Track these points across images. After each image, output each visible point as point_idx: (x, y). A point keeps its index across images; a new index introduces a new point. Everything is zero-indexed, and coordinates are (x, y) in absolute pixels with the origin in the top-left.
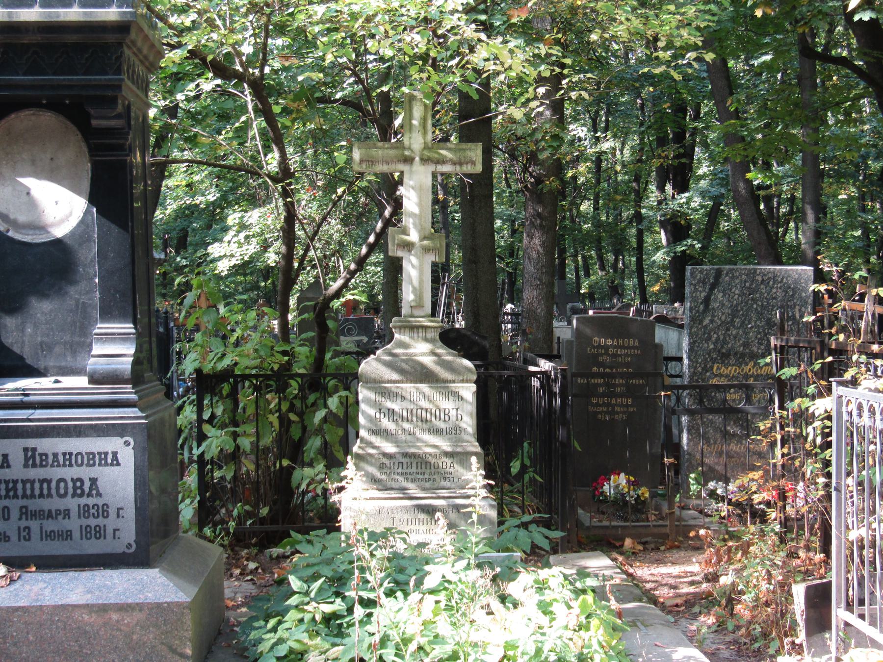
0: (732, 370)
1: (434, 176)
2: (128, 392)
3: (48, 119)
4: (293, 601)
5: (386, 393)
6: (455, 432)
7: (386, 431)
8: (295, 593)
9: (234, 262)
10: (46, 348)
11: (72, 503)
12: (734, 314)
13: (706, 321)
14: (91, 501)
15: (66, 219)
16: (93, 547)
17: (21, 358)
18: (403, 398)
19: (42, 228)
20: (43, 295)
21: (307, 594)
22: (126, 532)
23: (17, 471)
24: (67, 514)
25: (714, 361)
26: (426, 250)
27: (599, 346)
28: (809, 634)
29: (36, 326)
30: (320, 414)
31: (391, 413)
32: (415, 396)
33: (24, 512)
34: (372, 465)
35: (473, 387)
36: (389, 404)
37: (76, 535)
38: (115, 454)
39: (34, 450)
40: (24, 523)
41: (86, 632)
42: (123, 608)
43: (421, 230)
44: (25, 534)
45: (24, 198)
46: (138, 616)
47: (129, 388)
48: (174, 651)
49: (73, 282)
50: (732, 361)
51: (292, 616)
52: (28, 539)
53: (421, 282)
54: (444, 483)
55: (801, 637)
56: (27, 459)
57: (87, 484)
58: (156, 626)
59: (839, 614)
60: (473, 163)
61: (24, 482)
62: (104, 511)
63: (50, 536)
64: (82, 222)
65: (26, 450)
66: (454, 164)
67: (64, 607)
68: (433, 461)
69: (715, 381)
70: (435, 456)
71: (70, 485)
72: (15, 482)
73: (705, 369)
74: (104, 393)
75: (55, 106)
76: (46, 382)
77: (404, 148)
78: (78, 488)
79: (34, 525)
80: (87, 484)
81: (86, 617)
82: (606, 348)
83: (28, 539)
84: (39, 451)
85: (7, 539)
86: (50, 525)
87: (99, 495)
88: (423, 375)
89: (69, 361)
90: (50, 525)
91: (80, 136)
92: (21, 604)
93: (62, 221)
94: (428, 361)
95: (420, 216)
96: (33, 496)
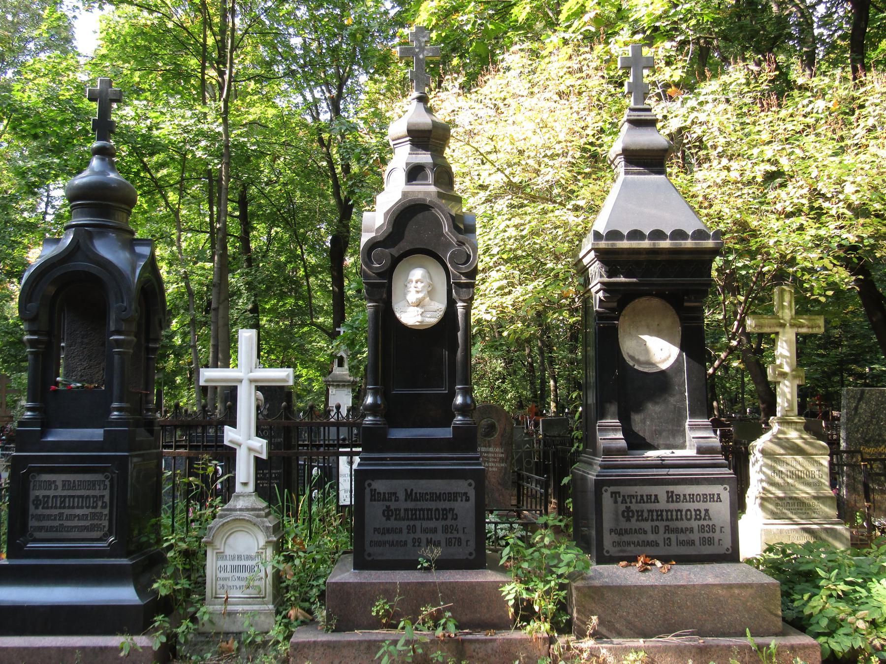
0: (871, 450)
1: (797, 334)
2: (720, 459)
3: (656, 302)
5: (777, 461)
6: (817, 485)
7: (778, 484)
8: (823, 578)
10: (658, 433)
11: (695, 524)
13: (856, 421)
14: (705, 523)
16: (707, 550)
17: (644, 439)
19: (653, 365)
20: (656, 403)
21: (829, 579)
23: (663, 505)
24: (691, 530)
25: (861, 444)
26: (795, 377)
29: (652, 420)
32: (794, 464)
33: (667, 529)
34: (771, 504)
35: (828, 458)
36: (779, 468)
37: (697, 543)
38: (718, 495)
39: (672, 492)
40: (667, 536)
41: (720, 601)
42: (741, 586)
47: (720, 456)
50: (872, 444)
53: (792, 396)
56: (668, 498)
57: (703, 513)
58: (761, 597)
60: (819, 327)
62: (713, 529)
63: (682, 543)
64: (677, 360)
65: (667, 492)
67: (707, 585)
70: (808, 499)
71: (693, 513)
72: (662, 511)
74: (706, 459)
75: (660, 295)
79: (673, 537)
80: (703, 513)
84: (676, 493)
85: (657, 545)
86: (682, 537)
89: (671, 441)
90: (682, 537)
91: (674, 312)
94: (799, 442)
95: (790, 358)
96: (672, 519)
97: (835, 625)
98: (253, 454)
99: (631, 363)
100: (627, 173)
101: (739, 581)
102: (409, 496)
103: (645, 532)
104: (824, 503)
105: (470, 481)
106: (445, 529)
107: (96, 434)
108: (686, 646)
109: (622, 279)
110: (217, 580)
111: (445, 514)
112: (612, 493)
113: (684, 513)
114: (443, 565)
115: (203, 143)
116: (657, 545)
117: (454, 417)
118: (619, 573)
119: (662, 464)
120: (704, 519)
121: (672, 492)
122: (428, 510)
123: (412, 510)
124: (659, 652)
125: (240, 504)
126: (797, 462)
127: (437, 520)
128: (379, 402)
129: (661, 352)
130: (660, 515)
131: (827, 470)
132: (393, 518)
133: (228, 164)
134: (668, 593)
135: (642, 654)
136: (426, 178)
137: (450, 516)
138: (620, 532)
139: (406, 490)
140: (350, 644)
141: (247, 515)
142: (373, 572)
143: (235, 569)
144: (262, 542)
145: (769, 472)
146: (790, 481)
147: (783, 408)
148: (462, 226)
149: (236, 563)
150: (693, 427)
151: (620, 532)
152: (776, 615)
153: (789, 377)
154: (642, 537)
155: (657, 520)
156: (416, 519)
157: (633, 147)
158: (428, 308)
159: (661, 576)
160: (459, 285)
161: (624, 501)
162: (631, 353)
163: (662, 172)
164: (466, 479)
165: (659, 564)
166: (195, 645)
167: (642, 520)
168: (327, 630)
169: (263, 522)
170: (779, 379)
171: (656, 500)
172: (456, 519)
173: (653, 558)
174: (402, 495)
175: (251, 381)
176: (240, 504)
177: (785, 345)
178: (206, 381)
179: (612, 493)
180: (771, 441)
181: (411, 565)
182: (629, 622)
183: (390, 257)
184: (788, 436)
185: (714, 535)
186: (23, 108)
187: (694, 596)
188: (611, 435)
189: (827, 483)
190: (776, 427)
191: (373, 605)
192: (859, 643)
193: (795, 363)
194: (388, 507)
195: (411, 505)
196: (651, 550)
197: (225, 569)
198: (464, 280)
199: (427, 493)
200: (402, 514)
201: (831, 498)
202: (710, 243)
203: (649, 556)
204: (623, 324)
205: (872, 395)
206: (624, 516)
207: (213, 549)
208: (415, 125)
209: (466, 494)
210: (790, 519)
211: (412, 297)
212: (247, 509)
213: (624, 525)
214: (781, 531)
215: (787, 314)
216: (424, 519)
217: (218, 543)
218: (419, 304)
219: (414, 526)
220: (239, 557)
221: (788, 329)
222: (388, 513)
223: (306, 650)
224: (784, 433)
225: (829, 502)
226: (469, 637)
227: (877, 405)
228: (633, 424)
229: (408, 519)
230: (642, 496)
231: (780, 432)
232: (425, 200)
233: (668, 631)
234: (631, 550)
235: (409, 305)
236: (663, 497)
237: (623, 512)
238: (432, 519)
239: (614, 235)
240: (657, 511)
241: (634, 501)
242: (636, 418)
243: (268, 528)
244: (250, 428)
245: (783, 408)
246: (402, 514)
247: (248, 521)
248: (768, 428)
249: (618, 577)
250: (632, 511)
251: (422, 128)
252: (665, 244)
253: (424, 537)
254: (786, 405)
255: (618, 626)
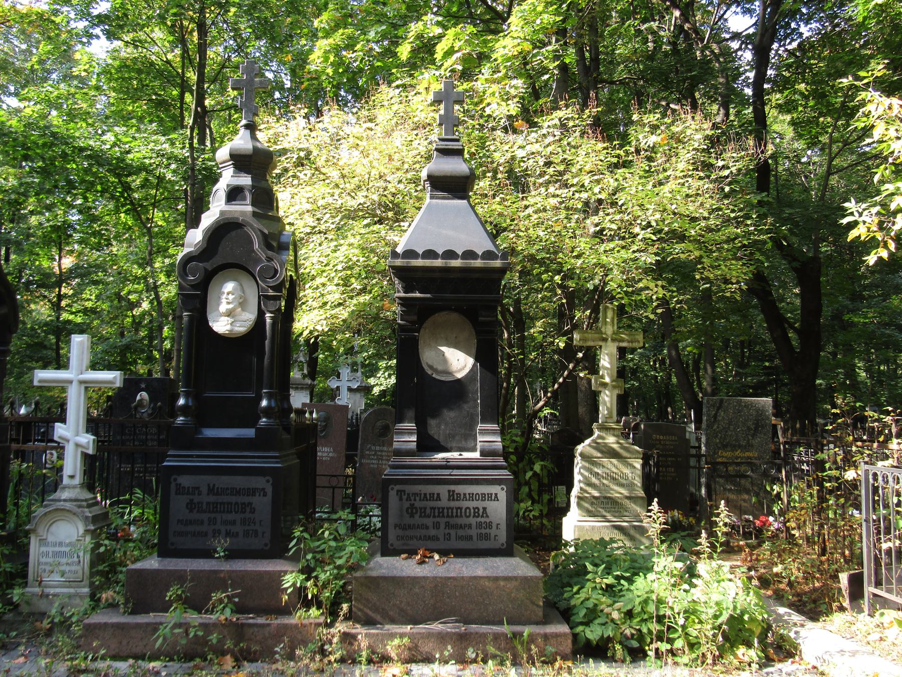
0: (729, 454)
2: (501, 461)
3: (454, 316)
4: (589, 576)
6: (630, 486)
8: (590, 572)
9: (382, 388)
10: (452, 436)
11: (473, 521)
12: (730, 423)
13: (715, 427)
14: (483, 520)
15: (463, 368)
17: (439, 442)
18: (603, 467)
19: (450, 373)
20: (451, 409)
21: (596, 573)
22: (501, 536)
23: (444, 502)
24: (470, 526)
25: (719, 448)
26: (614, 387)
27: (656, 440)
28: (851, 601)
30: (529, 474)
31: (597, 475)
32: (610, 466)
35: (641, 461)
36: (596, 470)
37: (475, 538)
38: (496, 494)
39: (454, 491)
40: (447, 531)
42: (507, 579)
43: (611, 376)
44: (448, 537)
45: (441, 357)
46: (514, 583)
48: (533, 603)
49: (466, 402)
50: (729, 449)
51: (589, 585)
52: (449, 540)
53: (611, 404)
54: (627, 514)
55: (846, 604)
57: (481, 510)
58: (524, 589)
59: (869, 589)
60: (639, 342)
61: (448, 509)
62: (489, 525)
63: (461, 538)
64: (471, 370)
65: (449, 491)
66: (629, 342)
67: (475, 578)
68: (620, 501)
69: (720, 460)
70: (621, 499)
72: (443, 508)
73: (714, 453)
74: (489, 461)
76: (455, 455)
77: (602, 333)
78: (476, 512)
80: (481, 510)
81: (487, 583)
82: (660, 440)
83: (449, 540)
85: (438, 539)
86: (461, 532)
87: (487, 516)
88: (612, 454)
90: (461, 532)
92: (452, 575)
93: (461, 370)
94: (615, 446)
95: (611, 369)
96: (452, 516)
97: (593, 614)
98: (80, 450)
99: (430, 372)
100: (431, 198)
101: (506, 574)
102: (211, 490)
103: (427, 528)
104: (635, 503)
105: (267, 478)
106: (244, 522)
107: (250, 433)
108: (448, 633)
109: (418, 295)
110: (39, 564)
111: (244, 507)
112: (398, 491)
113: (463, 510)
114: (233, 554)
115: (173, 166)
116: (438, 539)
117: (260, 418)
118: (397, 565)
119: (447, 465)
120: (482, 516)
121: (454, 491)
122: (228, 503)
123: (213, 503)
124: (422, 638)
125: (65, 495)
126: (611, 465)
127: (236, 513)
128: (190, 404)
129: (459, 362)
130: (441, 512)
131: (639, 473)
132: (195, 511)
133: (193, 185)
134: (439, 585)
135: (405, 640)
136: (244, 199)
137: (248, 510)
138: (404, 527)
139: (209, 485)
140: (138, 626)
141: (68, 505)
142: (174, 560)
143: (56, 554)
144: (81, 531)
145: (586, 474)
146: (605, 482)
147: (603, 415)
148: (275, 244)
149: (57, 549)
150: (484, 432)
151: (404, 527)
152: (538, 606)
153: (610, 387)
154: (424, 532)
155: (439, 516)
156: (217, 512)
157: (436, 174)
158: (238, 318)
159: (437, 568)
160: (268, 298)
161: (409, 499)
162: (430, 363)
163: (465, 197)
164: (264, 476)
165: (437, 557)
166: (13, 624)
167: (425, 516)
168: (125, 612)
169: (83, 512)
170: (600, 389)
171: (439, 498)
172: (253, 513)
173: (432, 551)
174: (204, 490)
175: (81, 382)
176: (65, 495)
177: (606, 358)
178: (40, 381)
179: (398, 491)
180: (589, 445)
181: (208, 554)
182: (402, 610)
183: (203, 271)
184: (606, 441)
185: (491, 531)
186: (11, 132)
187: (462, 587)
188: (406, 437)
189: (639, 485)
190: (597, 433)
191: (168, 590)
192: (609, 632)
193: (615, 374)
194: (192, 500)
195: (212, 499)
196: (431, 544)
197: (47, 554)
198: (271, 293)
199: (227, 489)
200: (204, 507)
201: (642, 498)
202: (497, 263)
203: (428, 550)
204: (423, 336)
205: (729, 404)
206: (408, 513)
207: (37, 536)
208: (236, 150)
209: (263, 489)
210: (604, 516)
211: (224, 307)
212: (71, 500)
213: (407, 520)
214: (593, 528)
215: (609, 330)
216: (224, 512)
217: (41, 530)
218: (229, 314)
219: (215, 518)
220: (61, 544)
221: (609, 343)
222: (191, 506)
223: (97, 631)
224: (603, 438)
225: (640, 501)
226: (251, 621)
227: (734, 413)
228: (429, 428)
229: (209, 512)
230: (425, 494)
231: (599, 437)
232: (238, 219)
233: (436, 619)
234: (413, 543)
235: (221, 316)
236: (444, 495)
237: (407, 509)
238: (231, 512)
239: (410, 254)
240: (439, 509)
241: (417, 498)
242: (432, 423)
243: (87, 517)
244: (78, 425)
245: (603, 415)
246: (204, 507)
247: (68, 511)
248: (591, 433)
249: (396, 568)
250: (416, 508)
251: (243, 153)
252: (456, 263)
253: (223, 529)
254: (606, 412)
255: (391, 613)
